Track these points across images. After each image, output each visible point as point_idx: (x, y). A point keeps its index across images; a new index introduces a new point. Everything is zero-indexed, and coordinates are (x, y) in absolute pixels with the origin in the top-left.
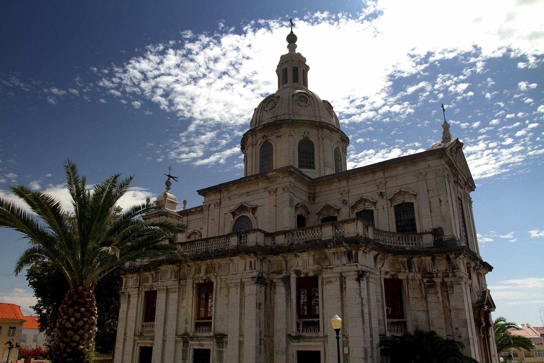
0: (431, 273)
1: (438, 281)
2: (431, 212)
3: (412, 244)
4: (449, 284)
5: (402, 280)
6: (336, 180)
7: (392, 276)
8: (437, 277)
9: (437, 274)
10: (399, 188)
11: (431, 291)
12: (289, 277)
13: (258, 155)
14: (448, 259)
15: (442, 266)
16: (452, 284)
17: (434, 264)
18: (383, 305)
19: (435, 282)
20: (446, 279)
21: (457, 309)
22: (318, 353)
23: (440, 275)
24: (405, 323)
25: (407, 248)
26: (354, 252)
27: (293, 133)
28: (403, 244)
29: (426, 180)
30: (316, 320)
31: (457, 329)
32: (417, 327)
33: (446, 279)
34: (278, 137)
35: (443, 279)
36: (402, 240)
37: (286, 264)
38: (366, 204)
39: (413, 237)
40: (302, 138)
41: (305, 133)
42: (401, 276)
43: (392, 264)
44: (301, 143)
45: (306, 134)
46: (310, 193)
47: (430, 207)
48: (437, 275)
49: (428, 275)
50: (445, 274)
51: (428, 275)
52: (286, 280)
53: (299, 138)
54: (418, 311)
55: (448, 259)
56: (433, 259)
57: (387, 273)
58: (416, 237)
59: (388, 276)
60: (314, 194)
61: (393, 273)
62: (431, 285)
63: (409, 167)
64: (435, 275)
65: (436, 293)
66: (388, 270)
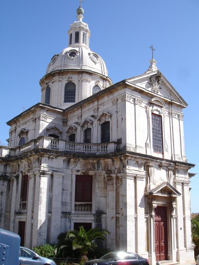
0: (110, 171)
1: (114, 176)
2: (117, 127)
3: (70, 149)
4: (120, 177)
5: (92, 176)
6: (76, 109)
7: (84, 173)
8: (114, 173)
9: (114, 171)
10: (102, 112)
11: (110, 183)
12: (19, 175)
13: (45, 95)
14: (121, 160)
15: (117, 164)
16: (122, 178)
17: (113, 164)
18: (71, 193)
19: (112, 177)
20: (119, 175)
21: (123, 196)
22: (25, 222)
23: (116, 172)
24: (91, 205)
25: (97, 154)
26: (40, 158)
27: (61, 79)
28: (72, 149)
29: (117, 105)
30: (78, 203)
31: (121, 209)
32: (99, 208)
33: (119, 175)
34: (52, 83)
35: (116, 175)
36: (72, 147)
37: (19, 167)
38: (88, 125)
39: (105, 146)
40: (67, 82)
41: (69, 78)
42: (91, 173)
43: (85, 165)
44: (67, 85)
45: (70, 78)
46: (63, 119)
47: (117, 124)
48: (114, 172)
49: (109, 172)
50: (119, 171)
51: (109, 172)
52: (17, 177)
53: (65, 82)
54: (101, 197)
55: (121, 160)
56: (113, 161)
57: (78, 171)
58: (92, 146)
59: (79, 173)
60: (67, 119)
61: (84, 171)
62: (110, 179)
63: (110, 96)
64: (113, 172)
65: (113, 184)
66: (79, 169)
